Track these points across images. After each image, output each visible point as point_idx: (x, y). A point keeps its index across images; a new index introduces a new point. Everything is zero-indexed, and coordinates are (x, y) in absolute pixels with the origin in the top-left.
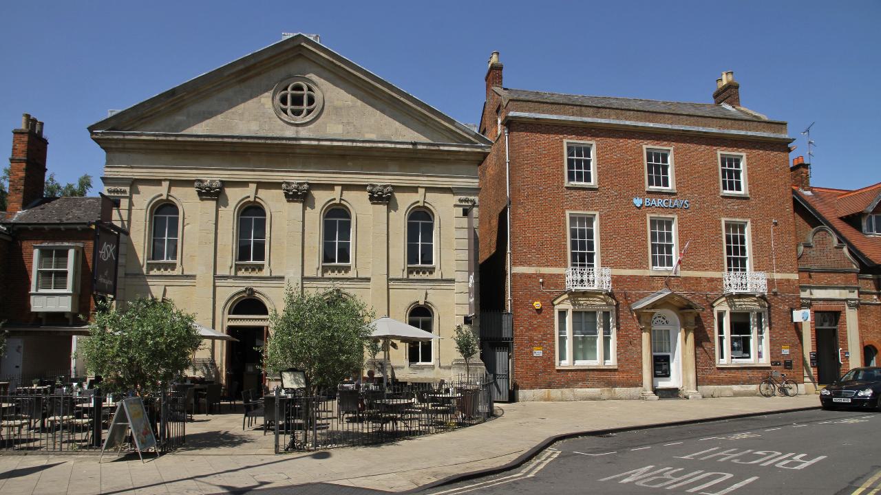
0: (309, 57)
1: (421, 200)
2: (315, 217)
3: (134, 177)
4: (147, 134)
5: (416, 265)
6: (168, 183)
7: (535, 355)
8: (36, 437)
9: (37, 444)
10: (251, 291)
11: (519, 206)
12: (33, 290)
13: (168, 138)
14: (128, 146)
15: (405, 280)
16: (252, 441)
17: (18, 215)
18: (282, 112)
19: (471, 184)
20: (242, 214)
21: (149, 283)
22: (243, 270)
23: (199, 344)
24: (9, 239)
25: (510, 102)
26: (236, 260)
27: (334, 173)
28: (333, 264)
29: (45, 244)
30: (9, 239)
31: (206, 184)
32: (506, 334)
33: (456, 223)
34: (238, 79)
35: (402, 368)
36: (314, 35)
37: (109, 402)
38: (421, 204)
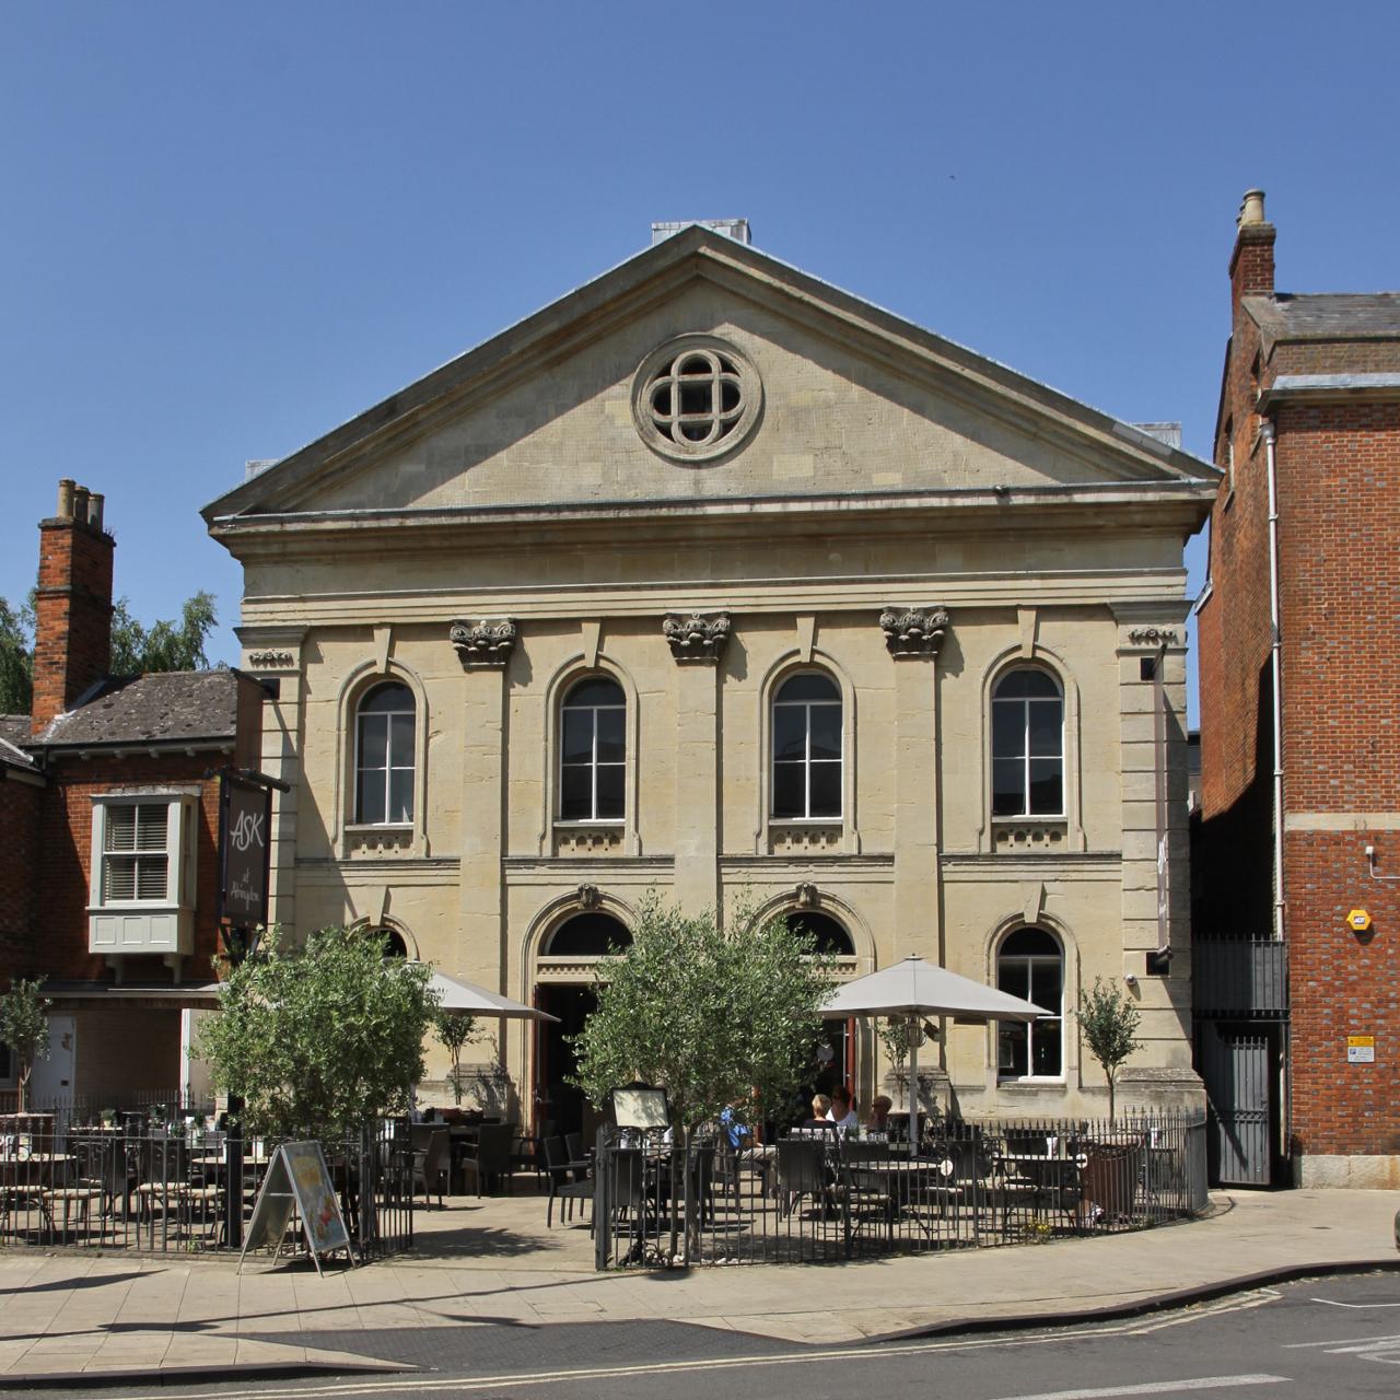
0: (721, 282)
1: (1028, 643)
2: (748, 701)
3: (308, 623)
4: (333, 517)
5: (1017, 818)
6: (387, 632)
7: (1351, 1058)
8: (117, 1228)
9: (120, 1239)
10: (593, 895)
11: (1304, 644)
12: (94, 904)
13: (384, 523)
14: (293, 547)
15: (985, 857)
16: (555, 1247)
17: (58, 724)
18: (659, 434)
19: (1167, 591)
20: (568, 702)
21: (347, 881)
22: (573, 842)
23: (468, 1028)
24: (40, 783)
25: (1278, 350)
26: (555, 819)
27: (793, 583)
28: (797, 820)
29: (117, 793)
30: (40, 783)
31: (476, 630)
32: (1264, 998)
33: (1123, 699)
34: (548, 356)
35: (980, 1090)
36: (734, 222)
37: (258, 1154)
38: (1026, 653)
